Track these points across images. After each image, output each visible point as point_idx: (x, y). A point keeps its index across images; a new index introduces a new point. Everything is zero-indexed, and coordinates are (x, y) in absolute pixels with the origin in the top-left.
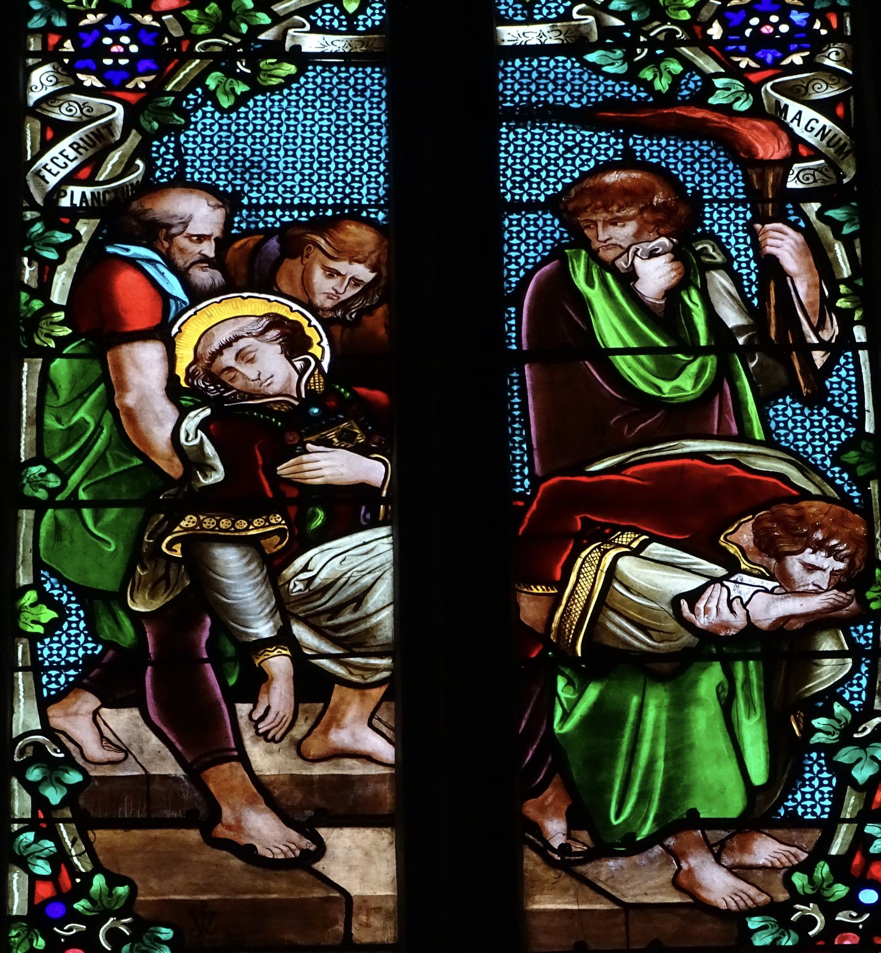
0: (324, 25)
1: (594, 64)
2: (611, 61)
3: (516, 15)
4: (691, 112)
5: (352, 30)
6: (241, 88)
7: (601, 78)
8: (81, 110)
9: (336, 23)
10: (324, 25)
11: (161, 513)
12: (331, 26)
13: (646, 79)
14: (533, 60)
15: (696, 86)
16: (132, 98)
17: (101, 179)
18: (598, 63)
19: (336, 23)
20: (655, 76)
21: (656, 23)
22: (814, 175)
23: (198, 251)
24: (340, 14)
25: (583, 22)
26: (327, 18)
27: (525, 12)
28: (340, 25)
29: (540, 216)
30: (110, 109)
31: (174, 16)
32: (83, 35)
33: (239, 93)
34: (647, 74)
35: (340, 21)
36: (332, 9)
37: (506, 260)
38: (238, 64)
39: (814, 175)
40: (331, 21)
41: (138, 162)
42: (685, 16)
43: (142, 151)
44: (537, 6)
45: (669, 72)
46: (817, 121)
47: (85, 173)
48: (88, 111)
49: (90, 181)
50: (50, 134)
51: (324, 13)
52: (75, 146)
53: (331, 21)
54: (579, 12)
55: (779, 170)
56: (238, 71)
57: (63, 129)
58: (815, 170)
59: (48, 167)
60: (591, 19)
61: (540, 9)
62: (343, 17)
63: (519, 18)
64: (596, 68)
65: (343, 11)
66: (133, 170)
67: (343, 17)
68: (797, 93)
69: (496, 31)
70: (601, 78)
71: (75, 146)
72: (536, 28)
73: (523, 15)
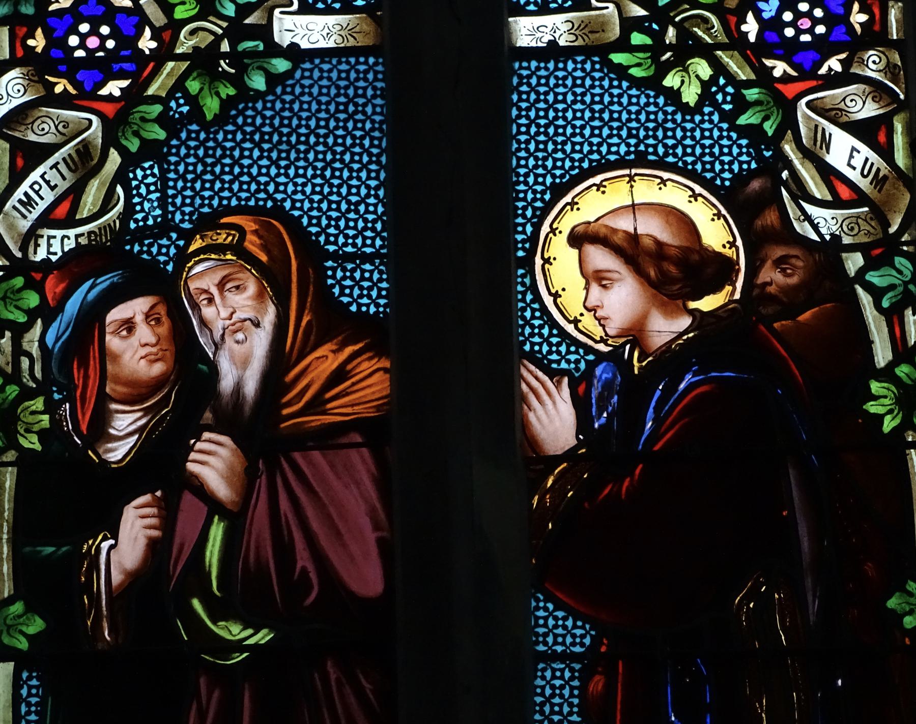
1: (620, 65)
2: (638, 61)
4: (96, 150)
7: (625, 84)
8: (56, 127)
13: (711, 76)
15: (134, 172)
16: (110, 109)
18: (625, 64)
20: (683, 82)
22: (857, 224)
23: (136, 344)
25: (605, 11)
33: (224, 96)
34: (672, 80)
37: (384, 159)
38: (222, 62)
39: (857, 224)
45: (697, 77)
47: (62, 211)
48: (64, 127)
49: (70, 222)
50: (20, 162)
55: (855, 222)
56: (220, 69)
57: (43, 152)
58: (858, 217)
59: (52, 241)
64: (621, 71)
69: (508, 22)
70: (625, 84)
72: (549, 20)
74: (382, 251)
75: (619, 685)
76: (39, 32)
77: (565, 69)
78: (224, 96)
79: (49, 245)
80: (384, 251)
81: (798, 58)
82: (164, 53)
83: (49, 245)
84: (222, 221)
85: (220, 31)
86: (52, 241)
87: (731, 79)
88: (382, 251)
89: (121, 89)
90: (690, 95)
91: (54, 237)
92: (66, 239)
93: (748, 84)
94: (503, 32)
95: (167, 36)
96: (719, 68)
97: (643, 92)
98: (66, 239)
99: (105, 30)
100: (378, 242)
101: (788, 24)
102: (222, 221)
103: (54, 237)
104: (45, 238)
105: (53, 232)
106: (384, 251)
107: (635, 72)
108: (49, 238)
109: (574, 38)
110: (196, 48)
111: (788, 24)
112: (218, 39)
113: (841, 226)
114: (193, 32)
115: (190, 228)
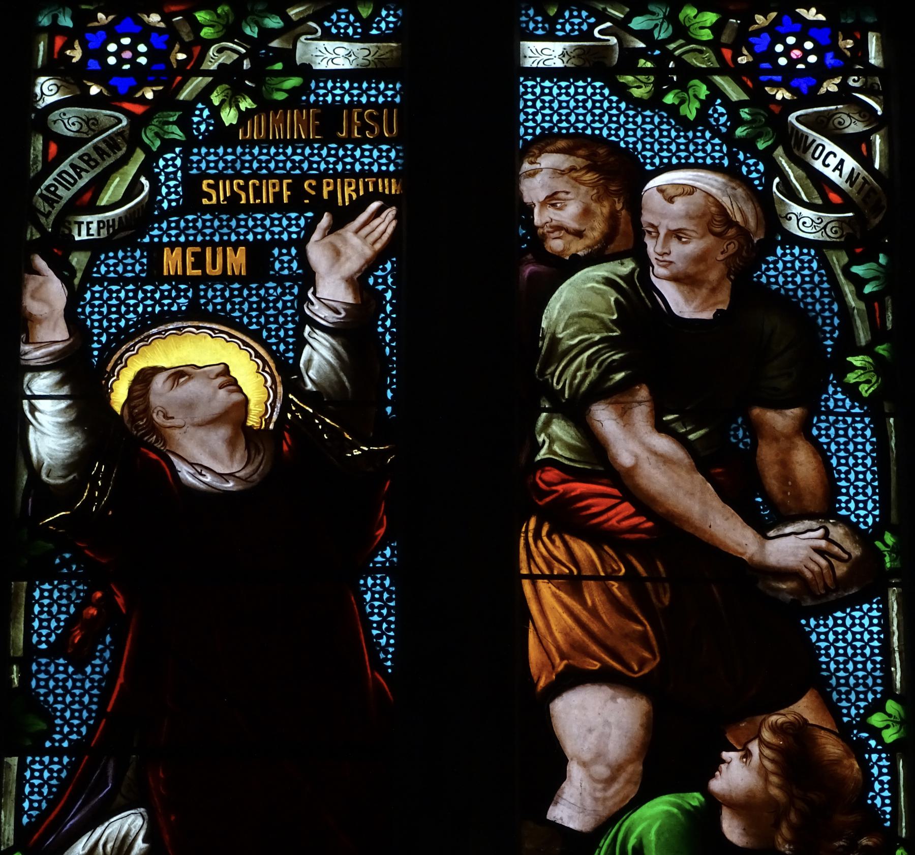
0: (339, 32)
3: (536, 28)
5: (365, 38)
6: (246, 104)
9: (350, 31)
10: (339, 32)
11: (4, 850)
12: (346, 34)
14: (325, 169)
16: (138, 109)
17: (103, 203)
19: (350, 31)
21: (681, 41)
24: (355, 21)
26: (342, 24)
27: (547, 26)
28: (355, 33)
29: (571, 84)
30: (114, 121)
31: (184, 18)
32: (89, 36)
33: (243, 109)
35: (355, 28)
36: (347, 15)
40: (346, 28)
41: (143, 180)
42: (707, 35)
43: (146, 169)
44: (561, 21)
46: (835, 156)
51: (339, 20)
52: (86, 158)
53: (346, 28)
54: (600, 32)
60: (613, 40)
61: (563, 25)
62: (358, 24)
63: (540, 32)
65: (358, 17)
66: (136, 191)
67: (358, 24)
68: (823, 125)
71: (86, 158)
73: (543, 28)
74: (142, 275)
75: (357, 613)
76: (77, 45)
77: (325, 88)
78: (243, 109)
79: (88, 229)
80: (144, 275)
81: (795, 83)
82: (193, 69)
83: (88, 229)
84: (865, 153)
85: (243, 51)
86: (91, 226)
87: (726, 102)
88: (142, 275)
89: (783, 97)
90: (690, 111)
91: (92, 223)
92: (832, 156)
93: (741, 104)
94: (515, 54)
95: (197, 50)
96: (716, 92)
97: (656, 113)
98: (832, 156)
99: (142, 48)
100: (138, 268)
101: (810, 52)
102: (865, 153)
103: (92, 223)
104: (85, 223)
105: (88, 218)
106: (144, 275)
107: (636, 93)
108: (89, 223)
109: (336, 51)
110: (221, 66)
111: (810, 52)
112: (242, 57)
113: (825, 228)
114: (220, 51)
115: (763, 163)
